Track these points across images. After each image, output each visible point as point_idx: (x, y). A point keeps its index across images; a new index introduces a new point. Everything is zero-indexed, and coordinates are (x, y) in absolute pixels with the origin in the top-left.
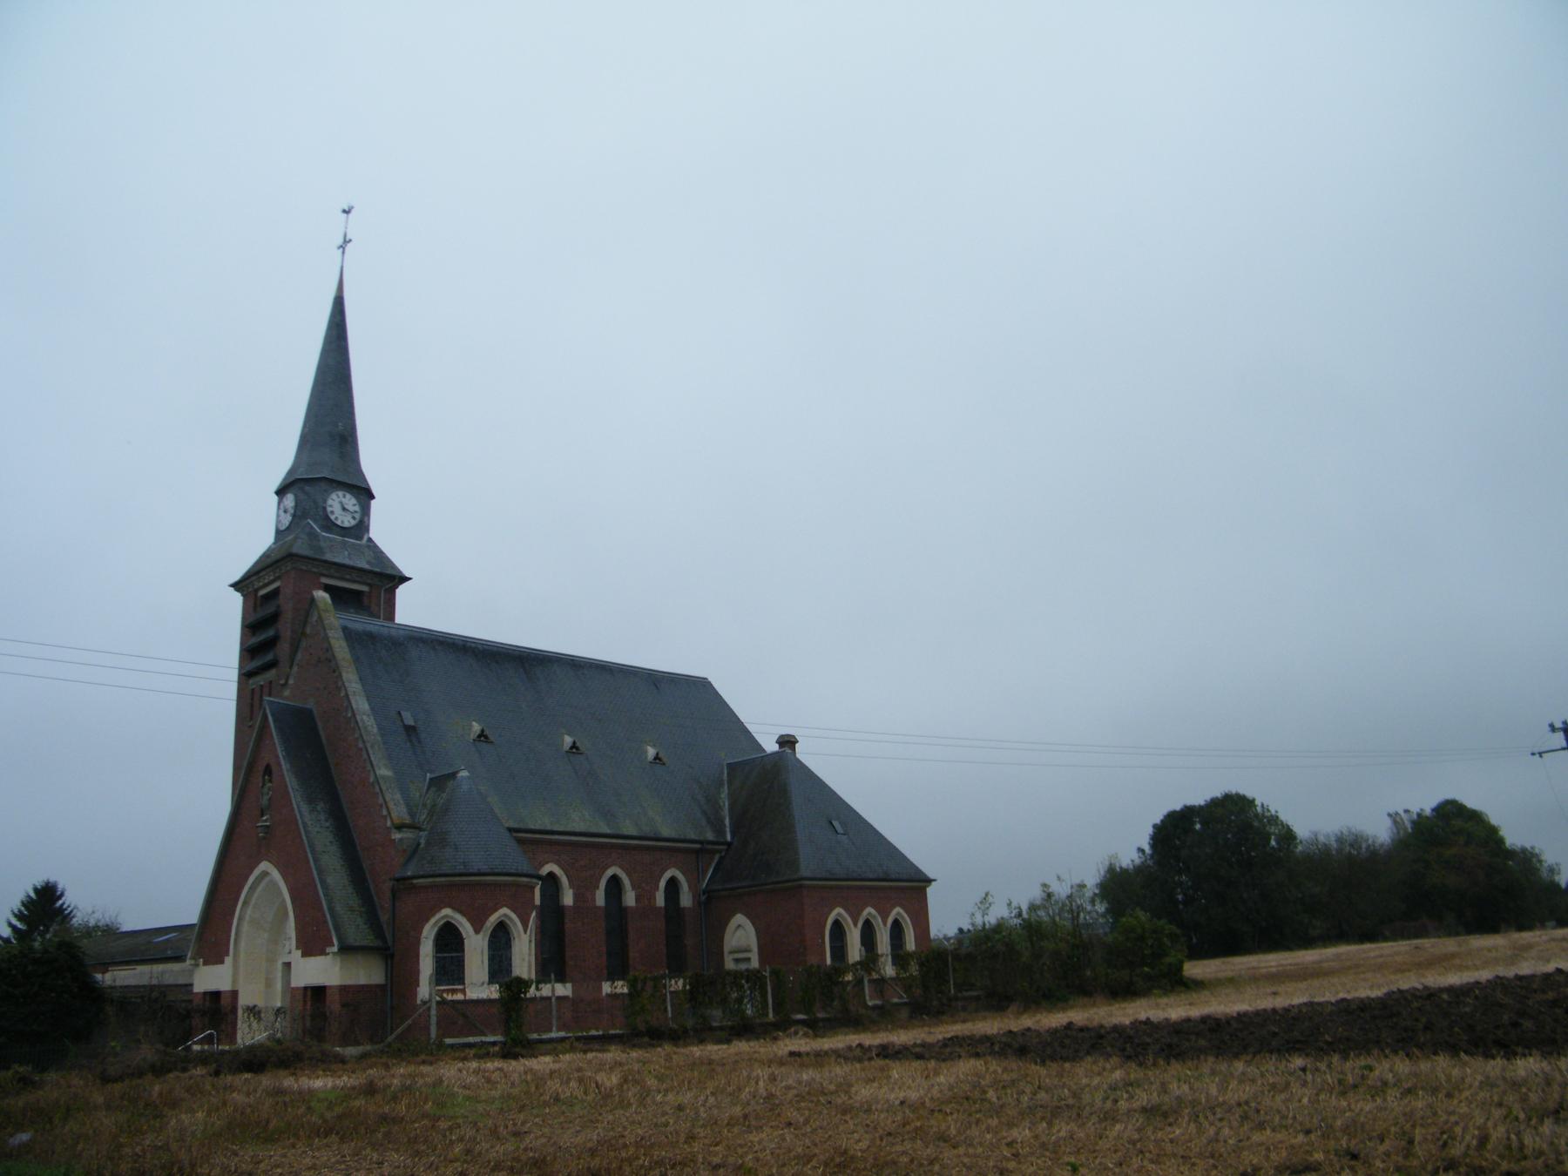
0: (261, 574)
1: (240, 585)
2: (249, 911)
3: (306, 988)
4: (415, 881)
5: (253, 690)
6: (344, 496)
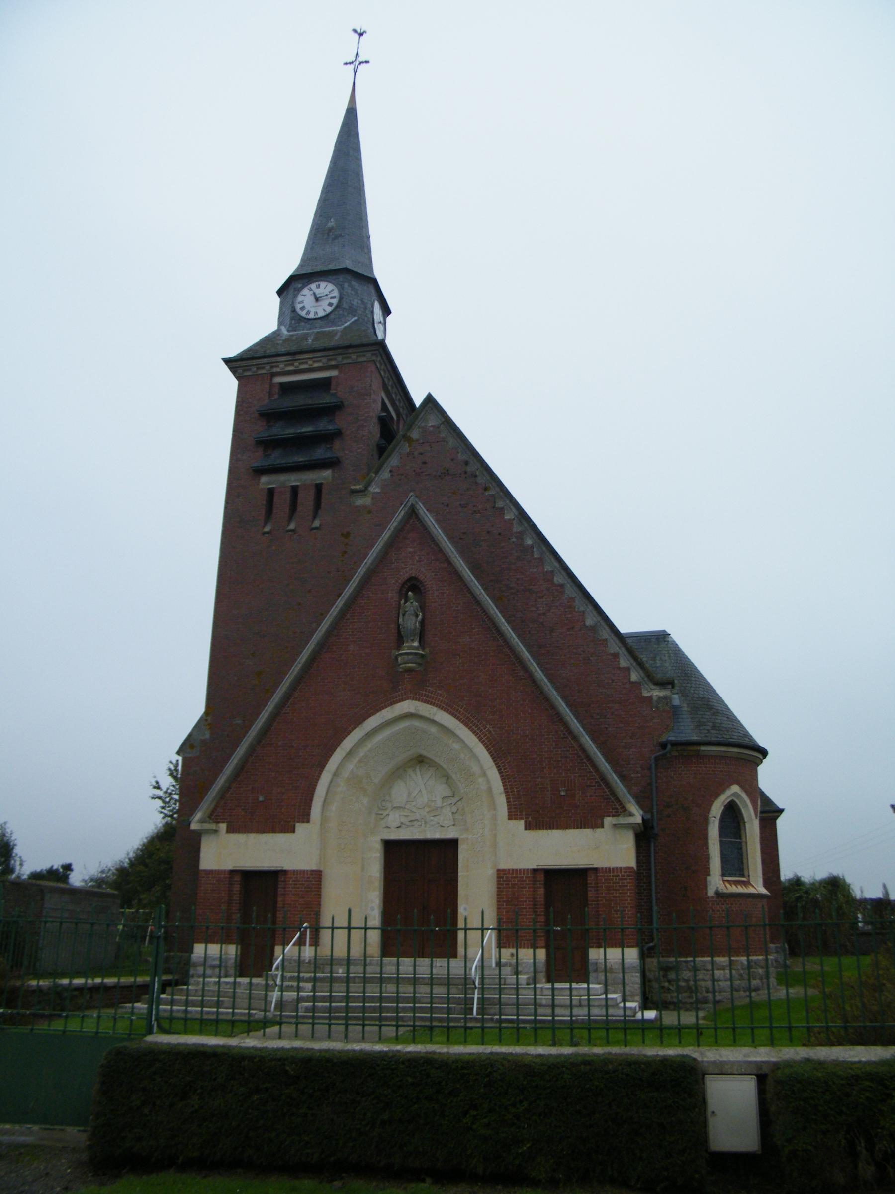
0: (298, 357)
1: (234, 364)
2: (350, 766)
3: (233, 872)
4: (703, 748)
5: (271, 492)
6: (330, 305)
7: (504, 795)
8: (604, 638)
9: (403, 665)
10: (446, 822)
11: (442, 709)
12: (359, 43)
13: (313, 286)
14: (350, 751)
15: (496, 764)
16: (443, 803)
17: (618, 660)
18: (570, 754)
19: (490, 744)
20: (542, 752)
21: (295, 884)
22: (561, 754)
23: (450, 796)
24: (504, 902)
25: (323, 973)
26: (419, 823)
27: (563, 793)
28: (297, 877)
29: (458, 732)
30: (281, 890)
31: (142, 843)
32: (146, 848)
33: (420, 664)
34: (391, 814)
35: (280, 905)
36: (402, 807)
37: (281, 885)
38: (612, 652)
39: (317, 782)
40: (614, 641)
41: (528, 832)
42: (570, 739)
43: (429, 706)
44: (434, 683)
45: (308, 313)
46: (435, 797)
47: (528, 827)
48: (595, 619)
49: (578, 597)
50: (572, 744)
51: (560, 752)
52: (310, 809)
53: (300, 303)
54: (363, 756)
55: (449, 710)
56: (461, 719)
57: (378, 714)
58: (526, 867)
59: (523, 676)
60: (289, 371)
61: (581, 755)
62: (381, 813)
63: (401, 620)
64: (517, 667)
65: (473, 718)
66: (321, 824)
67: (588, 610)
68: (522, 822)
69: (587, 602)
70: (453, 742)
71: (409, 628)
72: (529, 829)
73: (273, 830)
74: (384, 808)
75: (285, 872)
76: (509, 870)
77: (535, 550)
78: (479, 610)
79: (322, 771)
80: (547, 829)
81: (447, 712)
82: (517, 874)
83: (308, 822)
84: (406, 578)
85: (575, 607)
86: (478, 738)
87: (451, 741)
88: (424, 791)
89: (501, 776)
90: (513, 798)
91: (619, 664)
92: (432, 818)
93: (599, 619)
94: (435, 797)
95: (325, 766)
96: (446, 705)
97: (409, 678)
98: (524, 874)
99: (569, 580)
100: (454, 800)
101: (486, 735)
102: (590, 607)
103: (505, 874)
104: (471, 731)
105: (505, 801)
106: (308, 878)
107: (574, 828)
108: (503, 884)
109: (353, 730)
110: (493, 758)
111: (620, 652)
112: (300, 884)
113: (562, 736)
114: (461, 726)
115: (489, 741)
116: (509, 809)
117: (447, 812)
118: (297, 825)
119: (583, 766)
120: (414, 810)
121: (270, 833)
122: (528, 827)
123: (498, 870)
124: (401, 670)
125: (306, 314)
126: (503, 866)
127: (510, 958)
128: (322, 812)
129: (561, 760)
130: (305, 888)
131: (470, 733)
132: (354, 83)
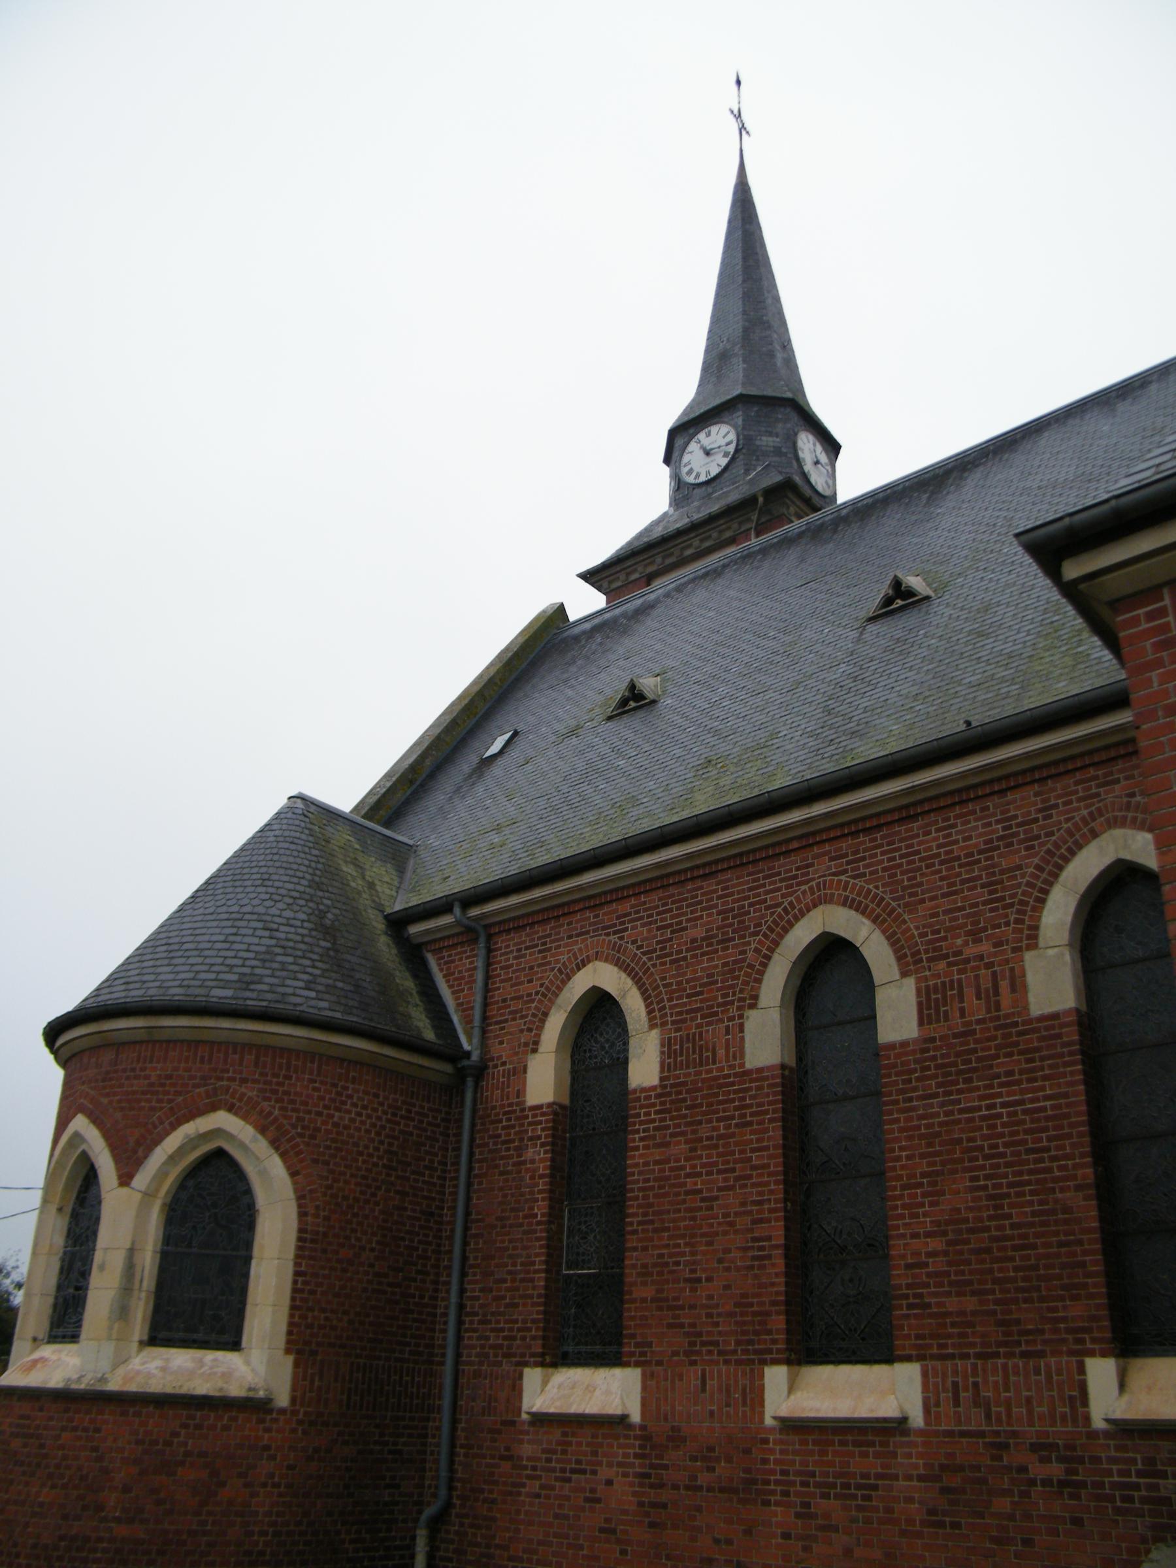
12: (739, 96)
13: (702, 436)
21: (1010, 827)
31: (280, 1353)
32: (299, 1352)
45: (698, 475)
53: (685, 466)
60: (708, 548)
125: (695, 478)
132: (741, 150)
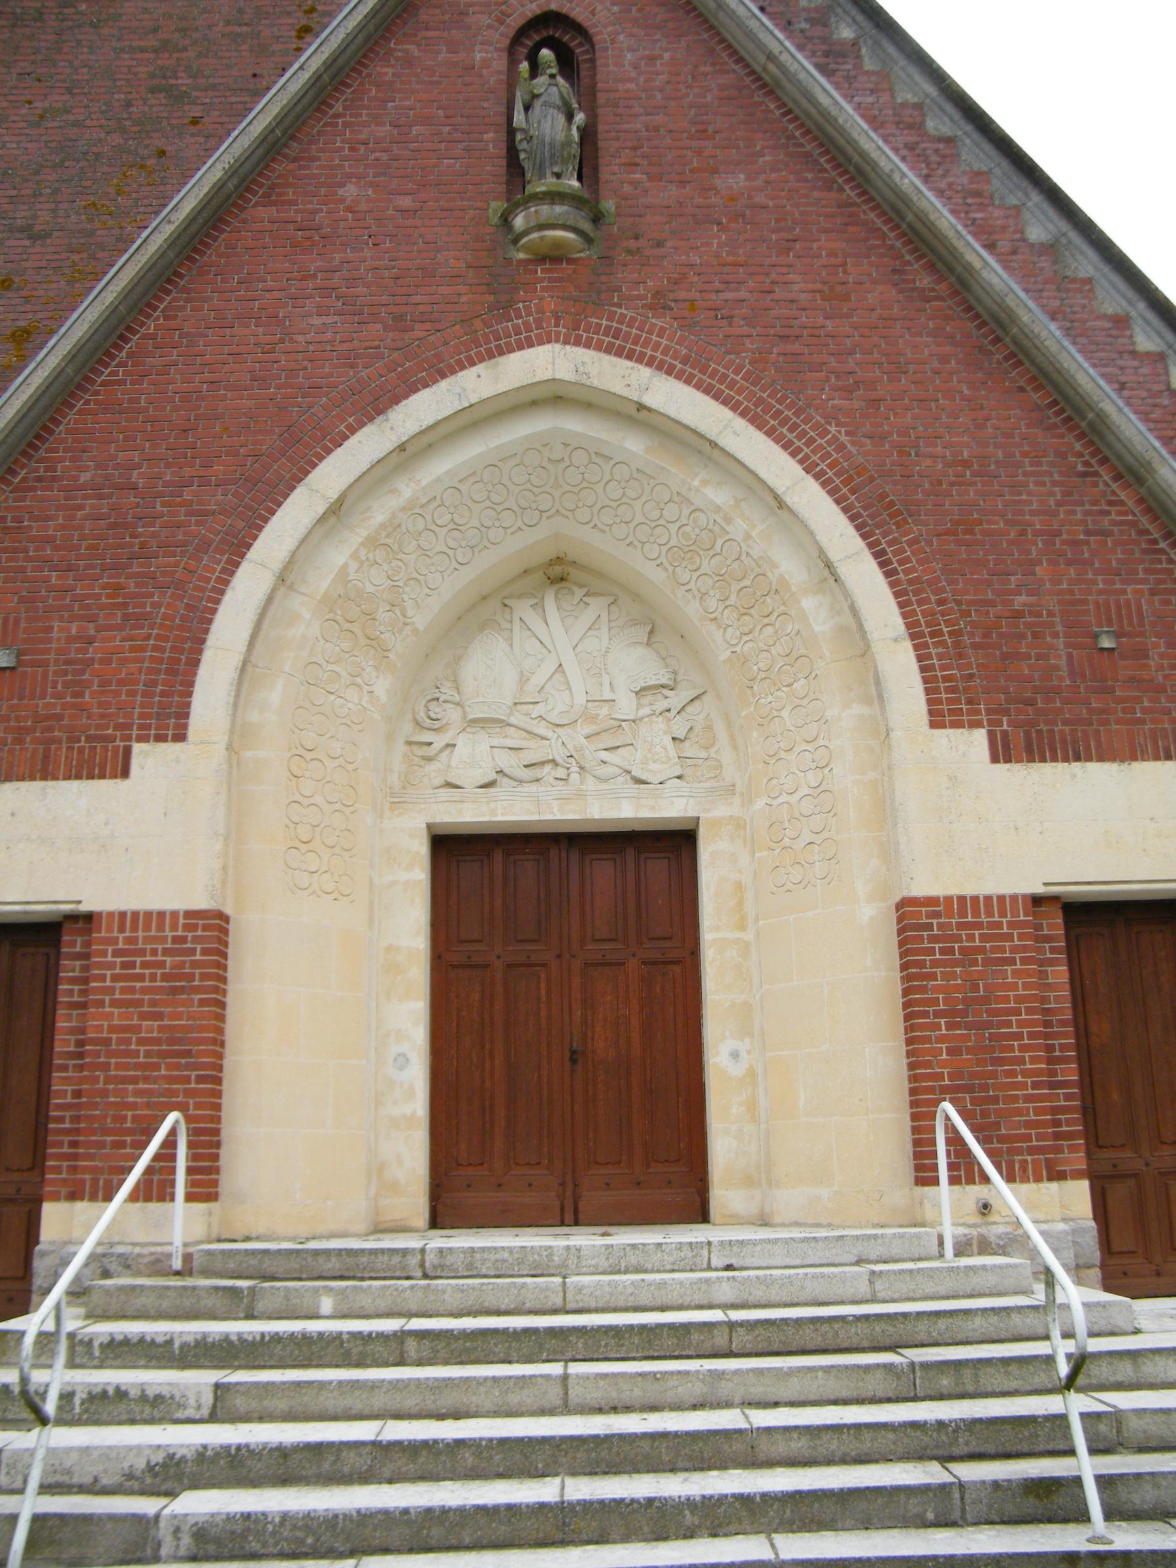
7: (908, 645)
8: (1082, 274)
9: (535, 235)
10: (653, 766)
11: (669, 372)
14: (341, 501)
15: (870, 546)
16: (639, 706)
17: (1128, 333)
18: (1114, 523)
19: (845, 483)
20: (1022, 513)
21: (125, 965)
22: (1084, 522)
23: (663, 686)
24: (937, 1014)
25: (250, 1316)
26: (561, 773)
27: (1106, 643)
28: (132, 940)
29: (728, 442)
30: (67, 991)
33: (588, 240)
34: (461, 742)
35: (63, 1043)
36: (501, 721)
37: (70, 969)
38: (1110, 311)
39: (218, 602)
40: (1111, 283)
41: (1002, 767)
42: (1107, 478)
43: (624, 364)
44: (640, 297)
46: (612, 690)
47: (1001, 752)
48: (1051, 227)
49: (997, 171)
50: (1114, 493)
51: (1079, 516)
52: (190, 694)
54: (383, 526)
55: (692, 376)
56: (739, 403)
57: (444, 384)
58: (1007, 890)
59: (933, 290)
61: (1150, 528)
62: (426, 737)
63: (519, 118)
64: (909, 263)
65: (780, 402)
66: (230, 747)
67: (1030, 204)
68: (980, 736)
69: (1025, 184)
70: (705, 483)
71: (547, 140)
72: (1008, 760)
73: (44, 770)
74: (437, 725)
75: (87, 920)
76: (948, 899)
77: (864, 51)
78: (772, 106)
79: (237, 565)
80: (1066, 759)
81: (688, 382)
82: (976, 913)
83: (180, 737)
84: (530, 15)
85: (992, 198)
86: (801, 462)
87: (696, 483)
88: (572, 670)
89: (892, 585)
90: (940, 657)
91: (1134, 343)
92: (605, 755)
93: (1064, 226)
94: (612, 690)
95: (249, 546)
96: (684, 362)
97: (551, 280)
98: (1003, 914)
99: (969, 128)
100: (676, 700)
101: (828, 455)
102: (1036, 198)
103: (937, 915)
104: (777, 441)
105: (914, 666)
106: (176, 940)
107: (1157, 758)
108: (931, 951)
109: (353, 430)
110: (858, 528)
111: (1133, 314)
112: (145, 965)
113: (1080, 468)
114: (740, 423)
115: (837, 474)
116: (930, 691)
117: (657, 734)
118: (137, 748)
119: (1160, 562)
120: (542, 729)
121: (32, 778)
122: (1001, 752)
123: (906, 906)
124: (522, 256)
126: (921, 888)
127: (977, 1219)
128: (235, 705)
129: (1087, 542)
130: (165, 977)
131: (776, 450)
